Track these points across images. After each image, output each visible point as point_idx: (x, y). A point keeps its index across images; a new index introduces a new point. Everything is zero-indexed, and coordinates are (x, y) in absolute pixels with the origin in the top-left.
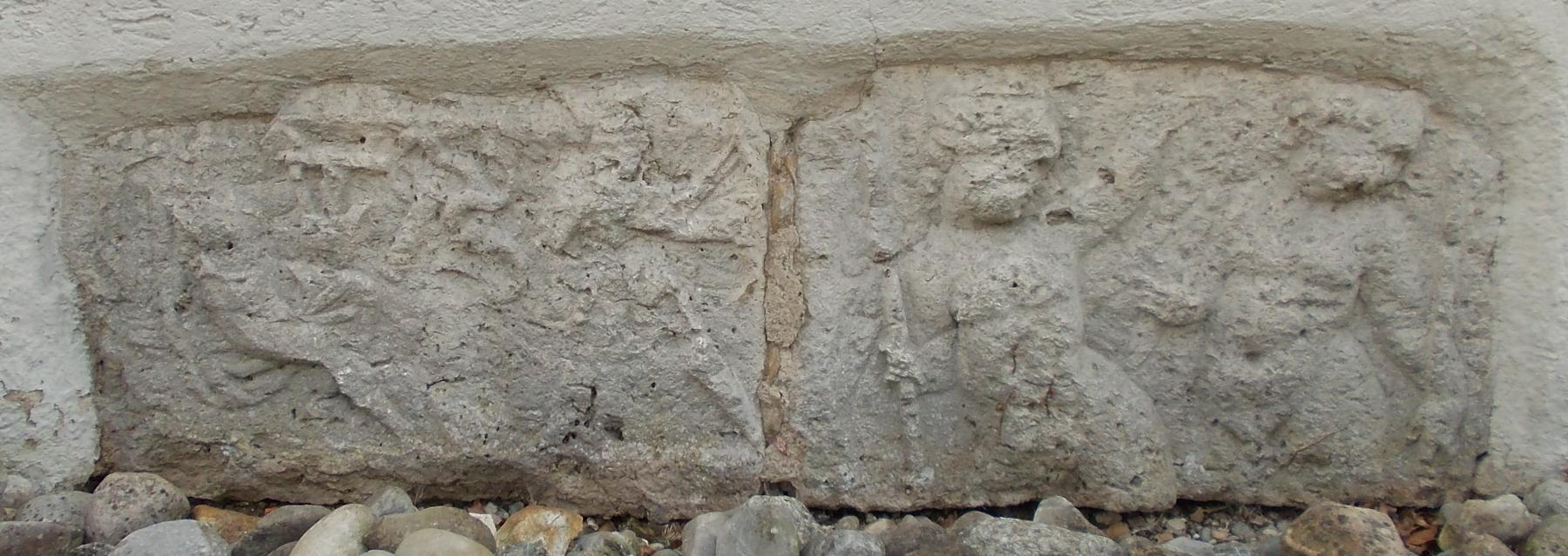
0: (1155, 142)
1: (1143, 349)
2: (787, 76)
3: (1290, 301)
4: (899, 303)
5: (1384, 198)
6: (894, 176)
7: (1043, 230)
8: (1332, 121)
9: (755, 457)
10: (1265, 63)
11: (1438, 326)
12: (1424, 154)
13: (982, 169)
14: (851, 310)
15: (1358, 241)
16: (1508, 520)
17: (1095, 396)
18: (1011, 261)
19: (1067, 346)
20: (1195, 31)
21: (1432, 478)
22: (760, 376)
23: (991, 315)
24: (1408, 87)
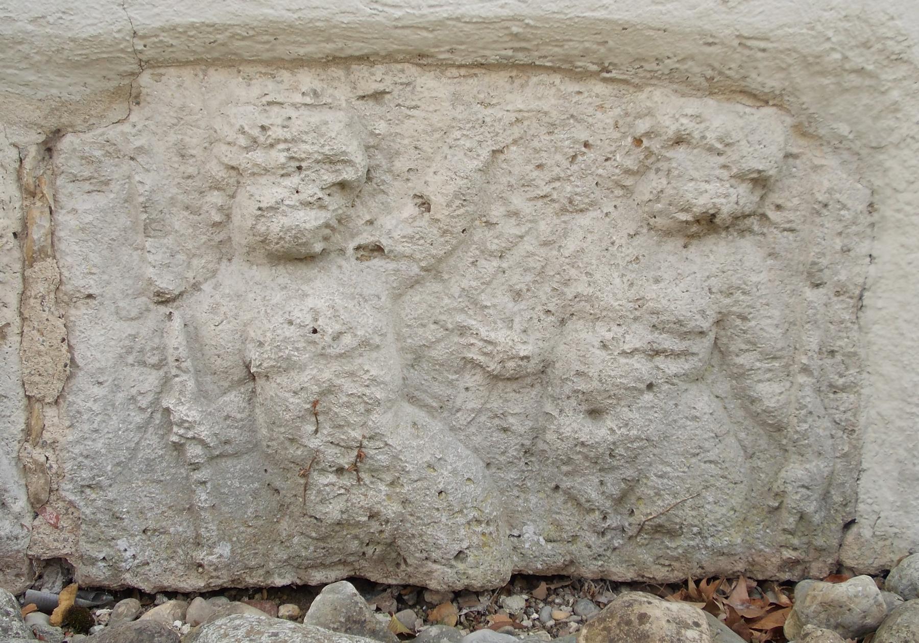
0: (476, 164)
1: (470, 405)
2: (31, 77)
3: (635, 351)
4: (183, 352)
5: (742, 233)
6: (173, 201)
7: (349, 265)
8: (679, 141)
9: (17, 531)
10: (603, 72)
11: (802, 379)
12: (787, 182)
13: (270, 192)
14: (130, 359)
15: (713, 281)
16: (858, 608)
17: (413, 461)
18: (310, 302)
19: (378, 403)
20: (515, 29)
21: (795, 549)
22: (20, 436)
23: (287, 366)
24: (767, 102)
